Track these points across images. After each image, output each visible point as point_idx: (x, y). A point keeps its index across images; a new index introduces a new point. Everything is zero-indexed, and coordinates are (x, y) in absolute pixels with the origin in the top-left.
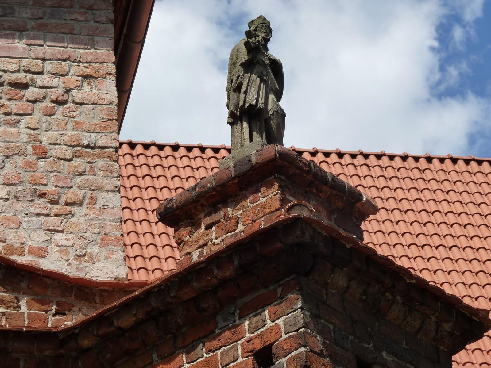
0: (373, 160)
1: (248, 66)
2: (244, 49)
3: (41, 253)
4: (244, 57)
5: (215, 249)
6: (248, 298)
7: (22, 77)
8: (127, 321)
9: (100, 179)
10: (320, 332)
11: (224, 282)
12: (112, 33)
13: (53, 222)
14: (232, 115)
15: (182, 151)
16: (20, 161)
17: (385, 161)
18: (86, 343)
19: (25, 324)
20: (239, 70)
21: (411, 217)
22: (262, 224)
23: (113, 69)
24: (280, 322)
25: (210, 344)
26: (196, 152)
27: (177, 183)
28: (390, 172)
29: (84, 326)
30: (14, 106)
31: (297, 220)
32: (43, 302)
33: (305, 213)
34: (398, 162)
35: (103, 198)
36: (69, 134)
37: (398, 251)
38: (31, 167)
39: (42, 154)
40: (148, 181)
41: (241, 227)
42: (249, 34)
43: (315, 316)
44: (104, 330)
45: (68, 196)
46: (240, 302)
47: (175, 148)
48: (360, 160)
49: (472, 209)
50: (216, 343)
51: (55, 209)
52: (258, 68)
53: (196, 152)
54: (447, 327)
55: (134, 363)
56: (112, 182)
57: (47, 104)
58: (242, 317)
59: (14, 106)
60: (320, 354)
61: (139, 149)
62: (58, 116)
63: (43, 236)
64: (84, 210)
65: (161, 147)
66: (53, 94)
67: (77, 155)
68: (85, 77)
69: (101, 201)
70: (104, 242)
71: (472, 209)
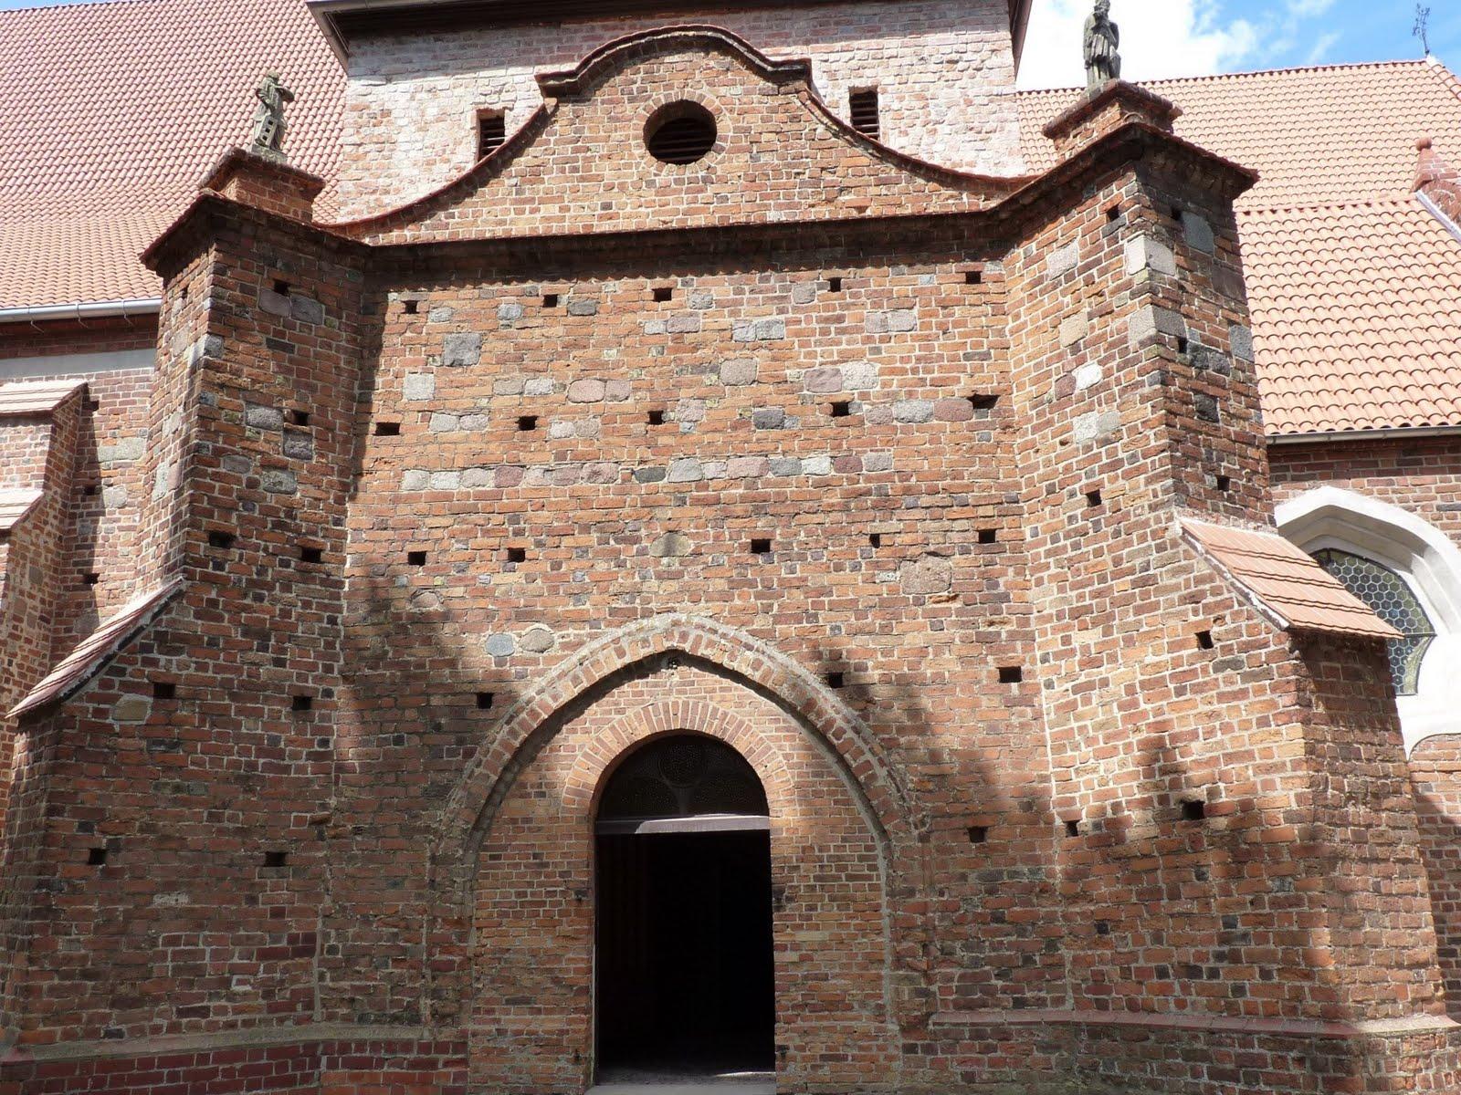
0: (1174, 84)
1: (1096, 29)
2: (1093, 18)
3: (972, 164)
4: (1093, 24)
5: (1080, 150)
6: (1102, 178)
7: (955, 56)
8: (1027, 200)
9: (1006, 115)
10: (1148, 194)
11: (1087, 170)
12: (1008, 20)
13: (979, 145)
14: (1087, 63)
15: (1052, 93)
16: (955, 109)
17: (1183, 83)
18: (1003, 216)
19: (966, 209)
20: (1090, 32)
21: (1200, 117)
22: (1109, 131)
23: (1010, 43)
24: (1123, 190)
25: (1079, 209)
26: (1061, 92)
27: (1050, 113)
28: (1186, 90)
29: (1002, 206)
30: (950, 76)
31: (1131, 125)
32: (976, 194)
33: (1136, 120)
34: (1191, 82)
35: (1008, 126)
36: (986, 89)
37: (1202, 140)
38: (963, 112)
39: (969, 103)
40: (1032, 115)
41: (1095, 134)
42: (1096, 8)
43: (1145, 185)
44: (1014, 207)
45: (987, 127)
46: (1098, 180)
47: (1048, 92)
48: (1166, 84)
49: (1241, 107)
50: (1083, 208)
51: (980, 136)
52: (1102, 30)
53: (1061, 92)
54: (1229, 182)
55: (1419, 6)
56: (1013, 116)
57: (971, 71)
58: (1098, 190)
59: (950, 76)
60: (1149, 208)
61: (1025, 95)
62: (978, 78)
63: (974, 154)
64: (997, 134)
65: (1039, 92)
66: (974, 65)
67: (991, 101)
68: (993, 51)
69: (1007, 129)
70: (1010, 154)
71: (1241, 107)
